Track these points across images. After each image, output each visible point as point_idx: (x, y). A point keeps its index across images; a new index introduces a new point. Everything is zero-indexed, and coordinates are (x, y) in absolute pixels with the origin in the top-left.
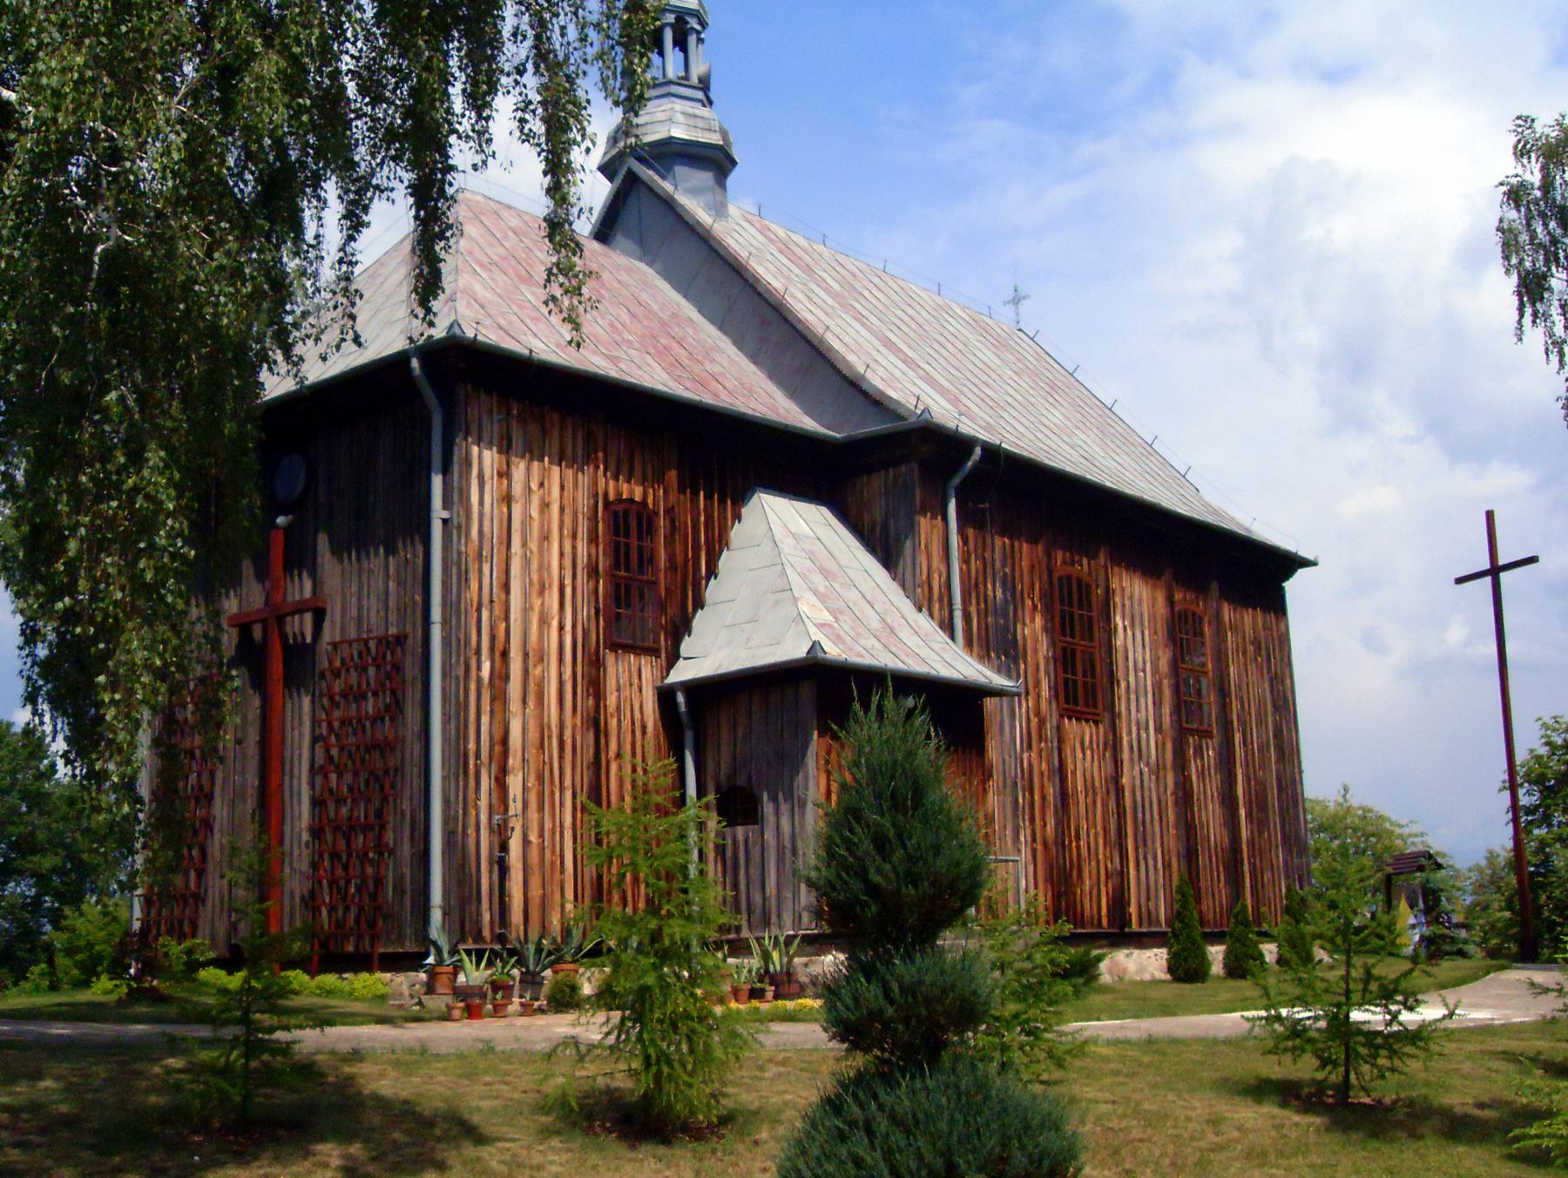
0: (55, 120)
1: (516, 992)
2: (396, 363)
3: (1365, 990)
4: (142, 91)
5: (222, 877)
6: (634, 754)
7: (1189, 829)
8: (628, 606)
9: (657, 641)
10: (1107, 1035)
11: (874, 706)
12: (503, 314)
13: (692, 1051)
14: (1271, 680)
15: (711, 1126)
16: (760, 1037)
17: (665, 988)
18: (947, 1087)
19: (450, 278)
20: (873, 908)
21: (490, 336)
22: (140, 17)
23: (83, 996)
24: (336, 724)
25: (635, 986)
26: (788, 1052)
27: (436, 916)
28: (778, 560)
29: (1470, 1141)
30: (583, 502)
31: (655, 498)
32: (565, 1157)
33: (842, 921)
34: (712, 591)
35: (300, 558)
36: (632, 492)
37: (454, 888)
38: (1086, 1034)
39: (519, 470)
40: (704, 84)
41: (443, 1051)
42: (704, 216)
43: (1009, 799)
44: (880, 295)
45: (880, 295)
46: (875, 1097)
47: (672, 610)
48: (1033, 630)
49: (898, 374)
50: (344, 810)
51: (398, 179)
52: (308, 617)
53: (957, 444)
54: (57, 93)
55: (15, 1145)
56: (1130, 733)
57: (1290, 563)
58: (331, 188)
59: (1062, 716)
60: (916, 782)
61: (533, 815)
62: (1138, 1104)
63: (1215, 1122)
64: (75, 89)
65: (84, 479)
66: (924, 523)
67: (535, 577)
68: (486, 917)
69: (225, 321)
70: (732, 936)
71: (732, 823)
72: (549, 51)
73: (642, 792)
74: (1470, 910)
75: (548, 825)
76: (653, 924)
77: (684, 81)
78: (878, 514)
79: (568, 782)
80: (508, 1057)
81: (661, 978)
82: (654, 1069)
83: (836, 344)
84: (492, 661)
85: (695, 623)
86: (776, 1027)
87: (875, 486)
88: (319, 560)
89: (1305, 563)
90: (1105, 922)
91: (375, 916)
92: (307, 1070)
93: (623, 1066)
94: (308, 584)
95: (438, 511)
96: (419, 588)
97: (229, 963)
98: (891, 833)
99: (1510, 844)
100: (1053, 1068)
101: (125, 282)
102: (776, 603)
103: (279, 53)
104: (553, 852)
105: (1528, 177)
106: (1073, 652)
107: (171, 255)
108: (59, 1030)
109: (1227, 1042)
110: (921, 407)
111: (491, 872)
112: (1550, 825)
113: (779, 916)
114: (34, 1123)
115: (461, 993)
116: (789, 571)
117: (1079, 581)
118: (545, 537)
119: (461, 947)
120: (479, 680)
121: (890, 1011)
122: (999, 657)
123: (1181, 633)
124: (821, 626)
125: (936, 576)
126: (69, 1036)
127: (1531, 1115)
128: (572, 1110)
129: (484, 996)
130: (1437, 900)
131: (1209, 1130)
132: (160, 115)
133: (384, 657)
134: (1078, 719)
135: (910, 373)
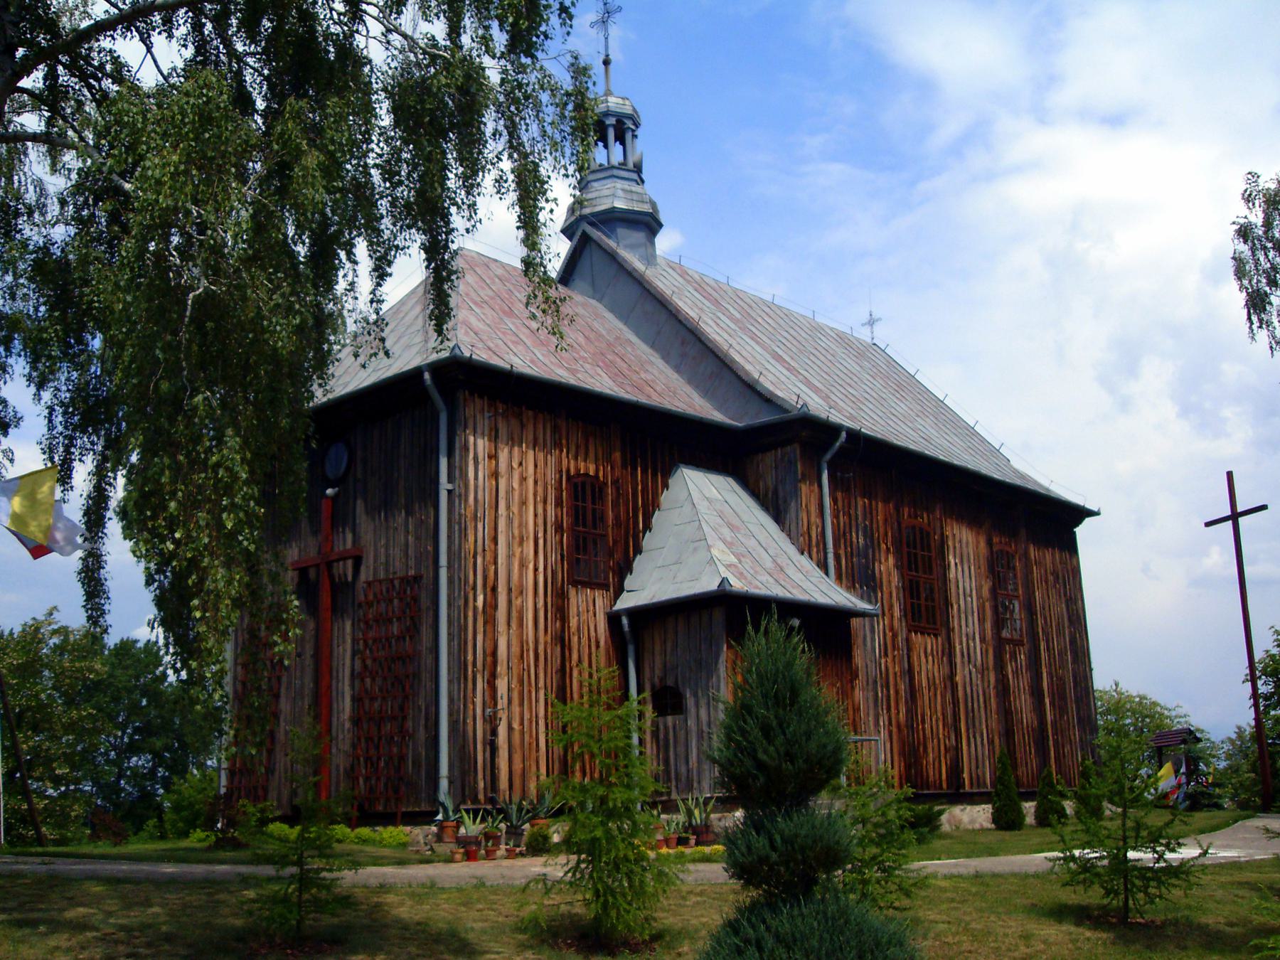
0: (157, 201)
1: (503, 840)
2: (416, 373)
3: (1137, 837)
4: (221, 180)
5: (286, 755)
7: (1007, 714)
9: (607, 578)
11: (762, 629)
12: (491, 338)
13: (631, 886)
14: (1067, 602)
15: (644, 942)
17: (610, 838)
18: (818, 913)
21: (482, 355)
22: (219, 127)
23: (184, 844)
24: (370, 642)
25: (589, 837)
26: (699, 887)
27: (444, 784)
28: (696, 519)
33: (740, 786)
34: (648, 541)
36: (587, 468)
38: (929, 870)
40: (638, 169)
41: (447, 886)
42: (639, 265)
43: (871, 694)
44: (770, 321)
45: (770, 321)
46: (764, 922)
47: (618, 556)
48: (887, 567)
49: (783, 378)
52: (350, 563)
53: (827, 430)
54: (159, 182)
56: (961, 643)
57: (1080, 514)
58: (361, 248)
59: (910, 631)
61: (516, 708)
62: (968, 924)
63: (1026, 937)
67: (516, 532)
68: (481, 785)
70: (664, 798)
73: (596, 691)
75: (527, 716)
77: (623, 165)
79: (541, 684)
80: (495, 890)
81: (608, 831)
82: (602, 899)
83: (737, 358)
85: (635, 565)
89: (1091, 513)
90: (945, 786)
92: (346, 901)
93: (580, 897)
94: (349, 537)
98: (774, 723)
99: (1253, 723)
100: (903, 897)
102: (695, 549)
104: (531, 736)
105: (1252, 219)
106: (918, 583)
108: (169, 869)
109: (1036, 876)
110: (801, 402)
113: (699, 782)
114: (143, 939)
115: (464, 842)
116: (703, 524)
117: (921, 530)
118: (523, 503)
119: (462, 807)
120: (475, 608)
121: (774, 856)
122: (861, 587)
124: (728, 566)
125: (814, 528)
128: (542, 930)
134: (922, 633)
135: (793, 377)
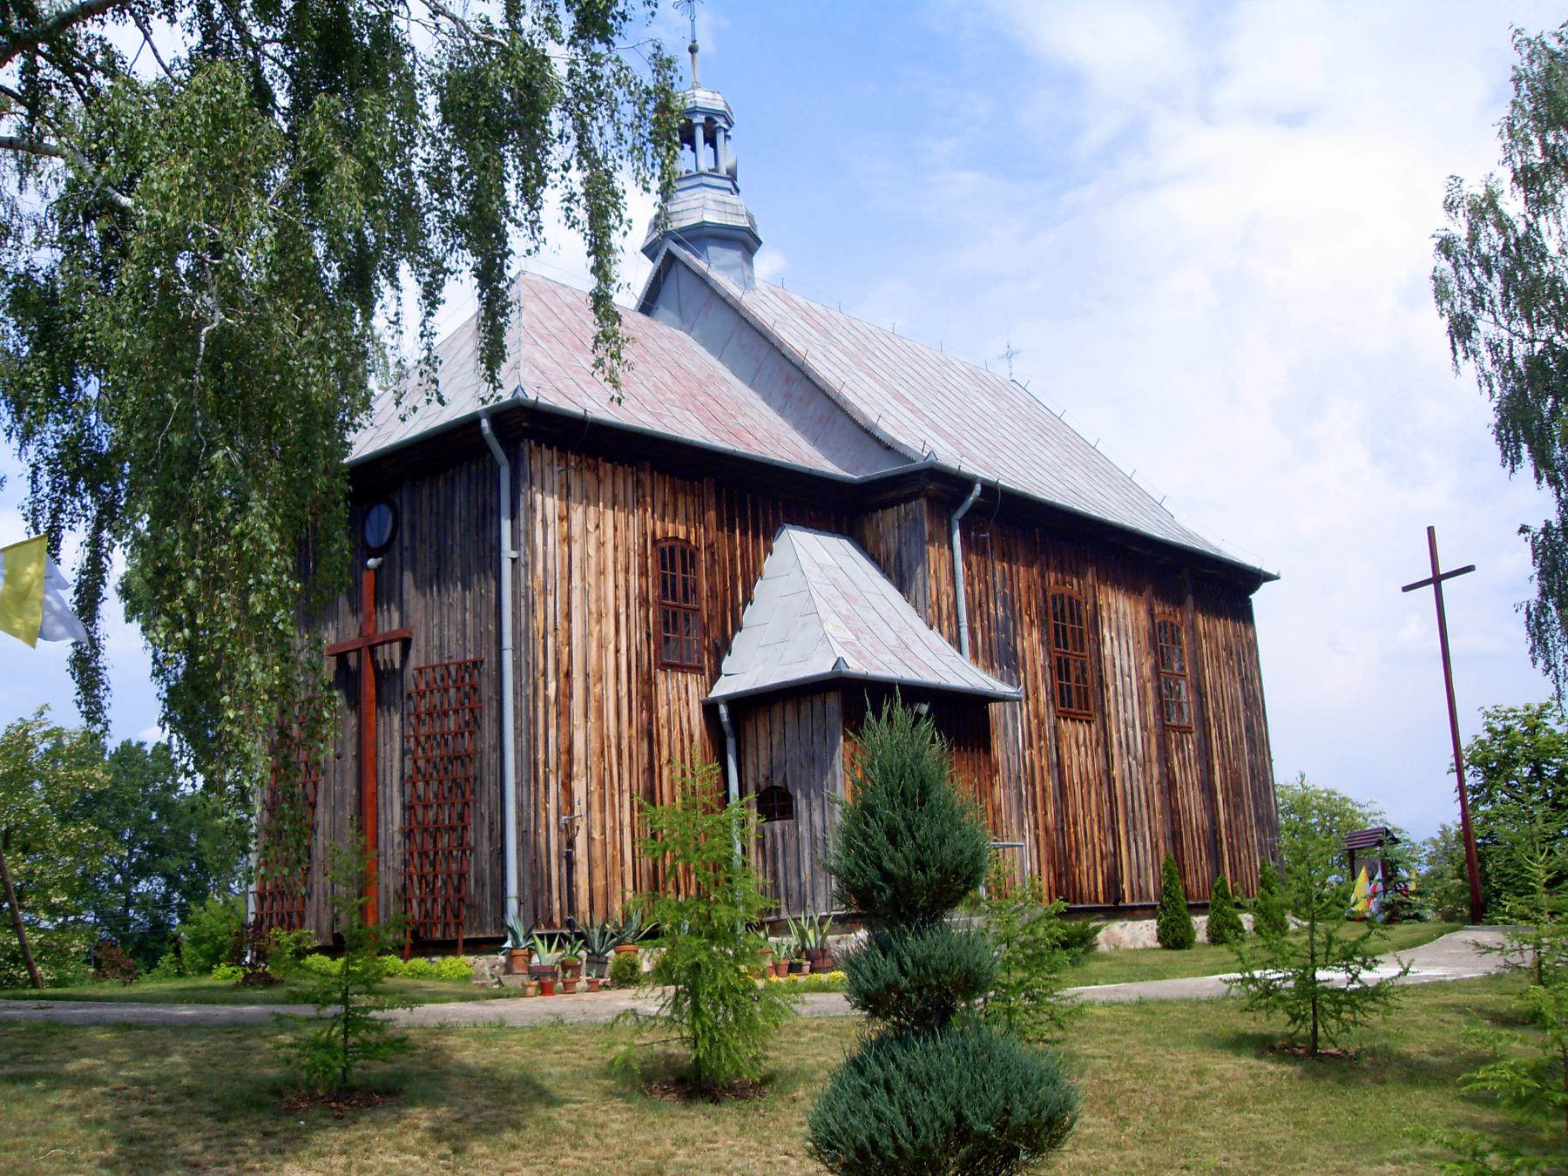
0: (164, 220)
1: (584, 970)
2: (472, 422)
3: (1327, 953)
6: (683, 761)
7: (1173, 813)
8: (675, 630)
9: (701, 660)
10: (1103, 997)
11: (884, 716)
13: (737, 1020)
14: (1242, 681)
16: (795, 1007)
19: (515, 349)
20: (888, 892)
21: (550, 398)
26: (818, 1023)
27: (513, 905)
29: (1426, 1085)
30: (634, 539)
31: (698, 536)
32: (625, 1116)
34: (749, 616)
35: (386, 591)
36: (676, 531)
37: (528, 881)
38: (1085, 997)
39: (577, 515)
40: (732, 175)
43: (1014, 792)
46: (893, 1059)
47: (714, 633)
48: (1031, 643)
49: (906, 422)
50: (431, 814)
51: (463, 263)
52: (397, 646)
54: (166, 198)
55: (143, 1115)
56: (1118, 731)
57: (1252, 579)
58: (404, 270)
60: (922, 781)
61: (596, 816)
62: (1130, 1058)
63: (1199, 1073)
64: (181, 193)
65: (197, 528)
66: (932, 551)
67: (593, 608)
68: (557, 905)
69: (314, 389)
70: (772, 918)
71: (770, 818)
72: (591, 150)
73: (689, 793)
74: (1424, 880)
75: (609, 824)
76: (702, 909)
78: (892, 543)
79: (626, 785)
80: (576, 1028)
83: (851, 398)
84: (558, 681)
86: (808, 997)
87: (888, 522)
88: (405, 597)
89: (1269, 577)
91: (459, 905)
92: (401, 1044)
93: (676, 1034)
95: (507, 552)
96: (492, 620)
97: (333, 950)
98: (902, 826)
99: (1459, 821)
101: (227, 357)
103: (357, 157)
107: (268, 333)
111: (560, 866)
112: (1493, 802)
116: (814, 595)
117: (1070, 598)
118: (601, 573)
119: (535, 932)
120: (546, 697)
121: (904, 982)
123: (1161, 641)
124: (844, 644)
126: (192, 1017)
127: (1478, 1061)
129: (555, 975)
130: (1395, 871)
131: (1193, 1080)
132: (255, 213)
133: (463, 679)
